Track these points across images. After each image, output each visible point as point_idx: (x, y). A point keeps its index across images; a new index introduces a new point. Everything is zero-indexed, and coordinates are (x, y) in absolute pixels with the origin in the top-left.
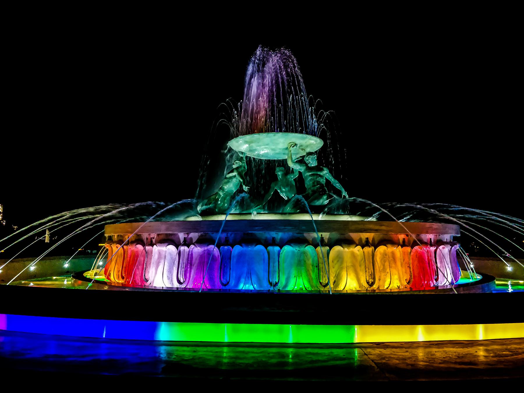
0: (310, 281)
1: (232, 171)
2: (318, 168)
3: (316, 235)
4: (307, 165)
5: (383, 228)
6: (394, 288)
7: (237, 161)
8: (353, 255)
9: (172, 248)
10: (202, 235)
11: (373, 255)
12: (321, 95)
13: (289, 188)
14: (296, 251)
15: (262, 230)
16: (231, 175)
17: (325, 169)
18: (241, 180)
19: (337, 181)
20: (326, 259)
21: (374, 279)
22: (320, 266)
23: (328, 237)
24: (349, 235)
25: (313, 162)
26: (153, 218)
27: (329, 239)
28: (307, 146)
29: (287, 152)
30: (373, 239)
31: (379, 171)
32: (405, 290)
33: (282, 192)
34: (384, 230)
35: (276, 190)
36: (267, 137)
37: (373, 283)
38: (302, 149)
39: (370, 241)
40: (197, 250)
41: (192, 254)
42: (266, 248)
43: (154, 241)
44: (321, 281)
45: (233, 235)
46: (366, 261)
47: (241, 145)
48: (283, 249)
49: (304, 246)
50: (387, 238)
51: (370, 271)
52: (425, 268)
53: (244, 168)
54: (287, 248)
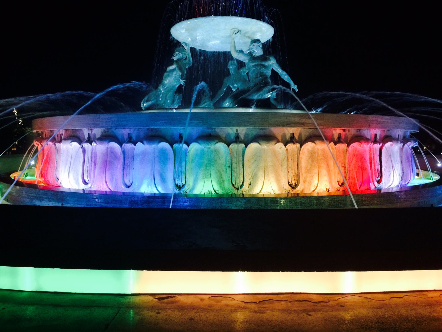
0: (221, 183)
2: (264, 58)
3: (231, 131)
6: (322, 191)
8: (274, 153)
9: (75, 144)
10: (105, 132)
14: (206, 149)
19: (285, 73)
20: (241, 158)
21: (298, 180)
22: (234, 167)
23: (244, 132)
25: (258, 52)
27: (246, 135)
30: (300, 135)
32: (339, 193)
37: (296, 186)
39: (296, 136)
40: (99, 148)
41: (96, 153)
42: (172, 146)
43: (63, 137)
44: (234, 183)
45: (136, 132)
46: (290, 160)
47: (182, 31)
48: (303, 147)
49: (214, 143)
51: (293, 171)
52: (365, 169)
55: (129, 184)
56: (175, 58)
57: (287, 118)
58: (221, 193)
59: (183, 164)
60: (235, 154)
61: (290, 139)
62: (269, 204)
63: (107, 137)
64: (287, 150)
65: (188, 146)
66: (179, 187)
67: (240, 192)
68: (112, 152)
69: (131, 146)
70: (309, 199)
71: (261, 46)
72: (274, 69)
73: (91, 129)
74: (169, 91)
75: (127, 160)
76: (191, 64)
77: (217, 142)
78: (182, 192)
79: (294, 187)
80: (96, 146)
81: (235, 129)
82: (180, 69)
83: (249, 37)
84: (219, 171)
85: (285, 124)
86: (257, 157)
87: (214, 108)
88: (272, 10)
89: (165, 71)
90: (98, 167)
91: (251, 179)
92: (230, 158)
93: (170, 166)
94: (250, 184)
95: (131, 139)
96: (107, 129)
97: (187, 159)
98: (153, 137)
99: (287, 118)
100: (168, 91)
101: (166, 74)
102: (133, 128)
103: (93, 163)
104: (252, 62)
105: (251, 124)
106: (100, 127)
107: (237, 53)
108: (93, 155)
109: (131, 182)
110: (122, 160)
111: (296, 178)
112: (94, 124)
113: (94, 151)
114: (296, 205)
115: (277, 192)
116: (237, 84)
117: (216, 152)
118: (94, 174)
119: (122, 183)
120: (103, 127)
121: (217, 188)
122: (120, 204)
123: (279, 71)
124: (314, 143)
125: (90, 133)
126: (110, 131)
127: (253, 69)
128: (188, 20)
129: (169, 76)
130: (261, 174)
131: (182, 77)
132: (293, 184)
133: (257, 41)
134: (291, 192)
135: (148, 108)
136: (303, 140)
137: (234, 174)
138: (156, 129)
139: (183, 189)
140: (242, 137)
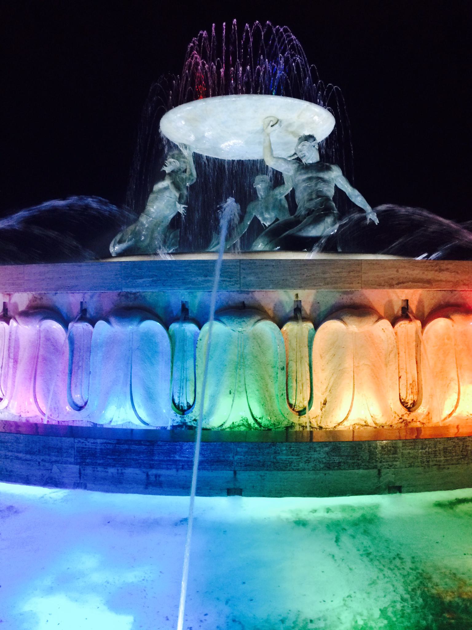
0: (265, 402)
2: (323, 164)
3: (285, 298)
8: (370, 339)
15: (154, 284)
19: (357, 192)
20: (306, 350)
24: (362, 295)
27: (316, 305)
30: (420, 302)
34: (447, 281)
35: (255, 218)
39: (413, 306)
41: (17, 341)
42: (167, 327)
44: (292, 401)
46: (402, 354)
48: (428, 327)
49: (252, 321)
50: (452, 301)
51: (409, 376)
55: (80, 403)
57: (397, 271)
58: (267, 423)
59: (190, 363)
61: (400, 312)
62: (379, 456)
63: (39, 310)
64: (396, 333)
65: (200, 328)
66: (182, 410)
67: (304, 420)
68: (48, 339)
69: (85, 327)
70: (461, 443)
71: (317, 147)
72: (339, 186)
73: (9, 295)
74: (157, 225)
75: (77, 357)
76: (195, 181)
77: (259, 321)
78: (187, 420)
79: (410, 408)
80: (17, 327)
81: (292, 293)
82: (177, 187)
83: (293, 133)
84: (262, 378)
85: (394, 282)
86: (336, 346)
87: (242, 253)
88: (331, 87)
89: (151, 191)
90: (21, 367)
91: (327, 393)
92: (284, 351)
93: (162, 367)
94: (325, 404)
95: (85, 314)
96: (40, 294)
97: (197, 355)
98: (131, 309)
99: (397, 271)
100: (155, 225)
101: (152, 197)
102: (90, 293)
103: (12, 361)
106: (25, 291)
108: (13, 344)
109: (85, 400)
110: (67, 355)
111: (415, 391)
112: (13, 284)
113: (13, 337)
114: (435, 456)
115: (381, 420)
116: (269, 214)
117: (257, 339)
118: (14, 382)
119: (66, 401)
120: (30, 290)
121: (258, 412)
122: (57, 456)
124: (451, 319)
125: (7, 301)
126: (44, 298)
127: (304, 185)
128: (188, 104)
129: (156, 198)
130: (347, 382)
131: (180, 200)
132: (410, 402)
133: (310, 138)
134: (405, 417)
135: (120, 255)
136: (426, 314)
137: (292, 384)
138: (135, 294)
139: (190, 415)
140: (307, 308)
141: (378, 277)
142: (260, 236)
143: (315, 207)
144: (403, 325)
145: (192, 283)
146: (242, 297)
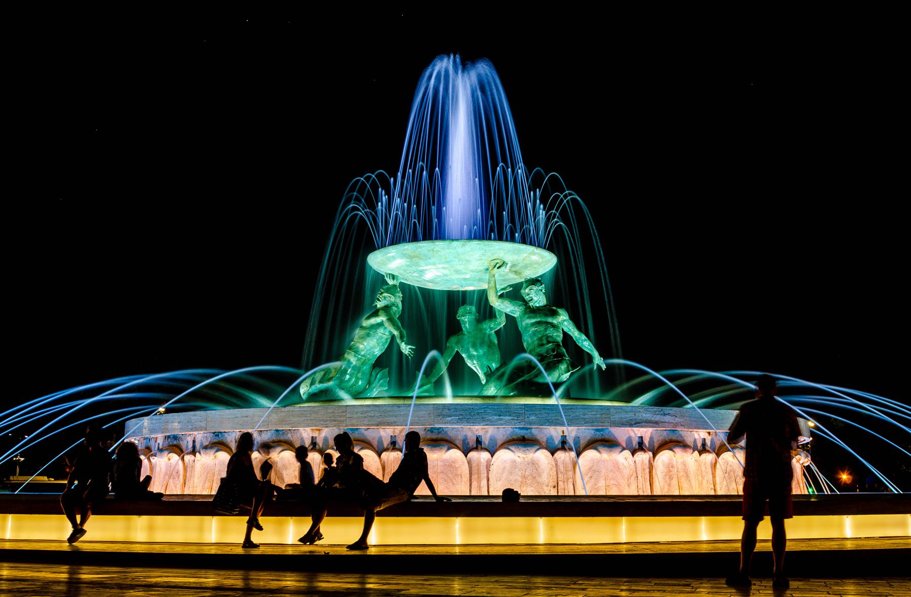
1: (376, 313)
2: (549, 311)
3: (555, 432)
4: (525, 303)
5: (667, 418)
7: (385, 294)
8: (617, 466)
9: (175, 457)
11: (651, 467)
12: (555, 160)
13: (486, 349)
14: (518, 460)
15: (460, 421)
16: (373, 321)
17: (561, 311)
18: (396, 333)
23: (573, 434)
25: (538, 298)
26: (280, 402)
27: (577, 440)
28: (526, 267)
29: (487, 277)
30: (651, 438)
31: (640, 318)
33: (471, 357)
36: (448, 248)
38: (516, 272)
39: (646, 442)
46: (639, 477)
47: (391, 262)
48: (657, 457)
50: (674, 438)
53: (397, 306)
54: (504, 456)
56: (379, 305)
60: (561, 468)
72: (566, 330)
81: (560, 429)
104: (529, 318)
105: (586, 422)
107: (500, 300)
116: (476, 350)
117: (534, 464)
123: (575, 333)
125: (316, 434)
140: (486, 441)
141: (622, 418)
142: (493, 379)
143: (547, 352)
144: (560, 455)
145: (488, 420)
146: (523, 432)
